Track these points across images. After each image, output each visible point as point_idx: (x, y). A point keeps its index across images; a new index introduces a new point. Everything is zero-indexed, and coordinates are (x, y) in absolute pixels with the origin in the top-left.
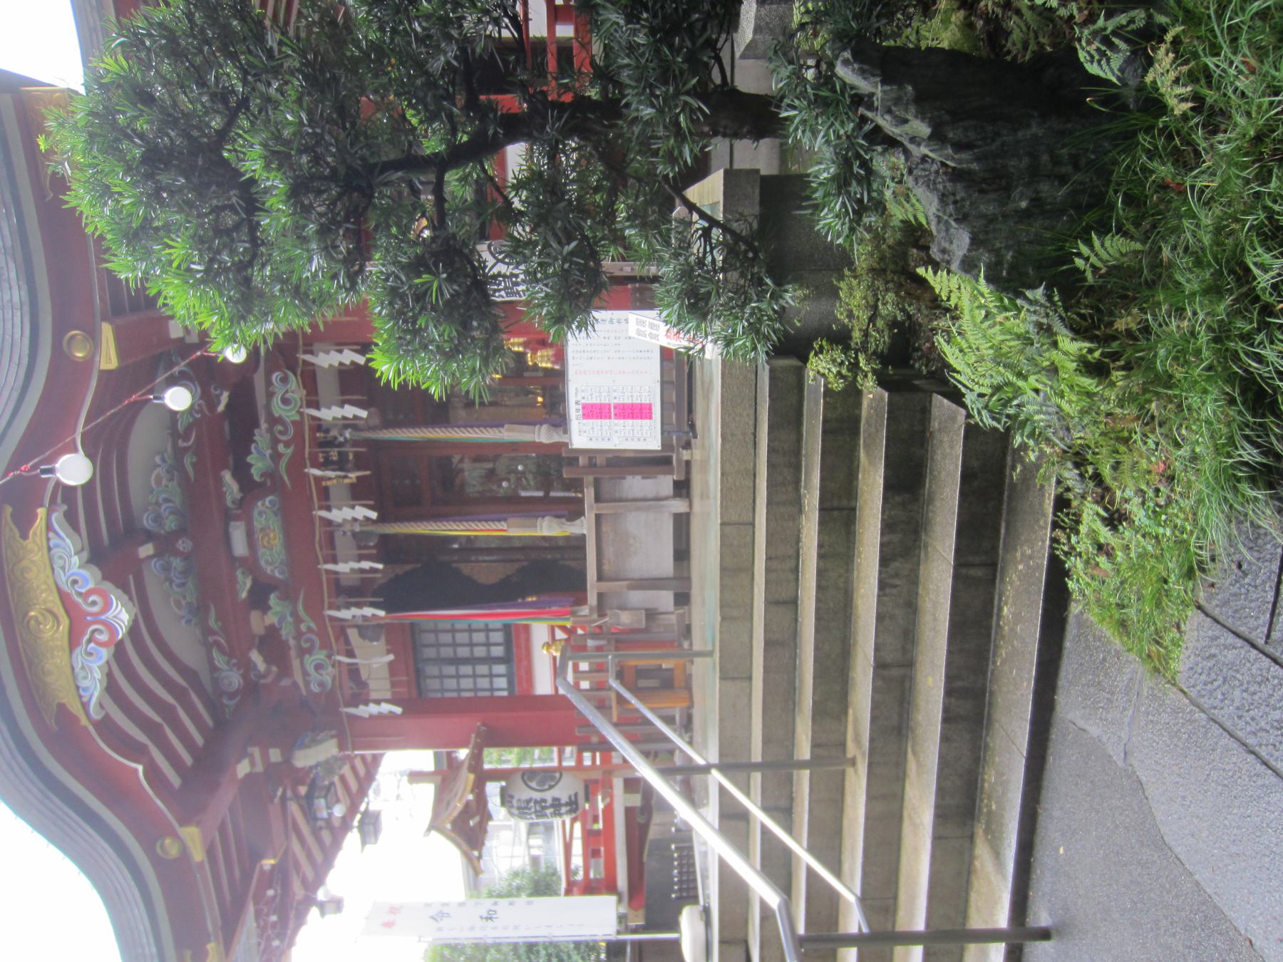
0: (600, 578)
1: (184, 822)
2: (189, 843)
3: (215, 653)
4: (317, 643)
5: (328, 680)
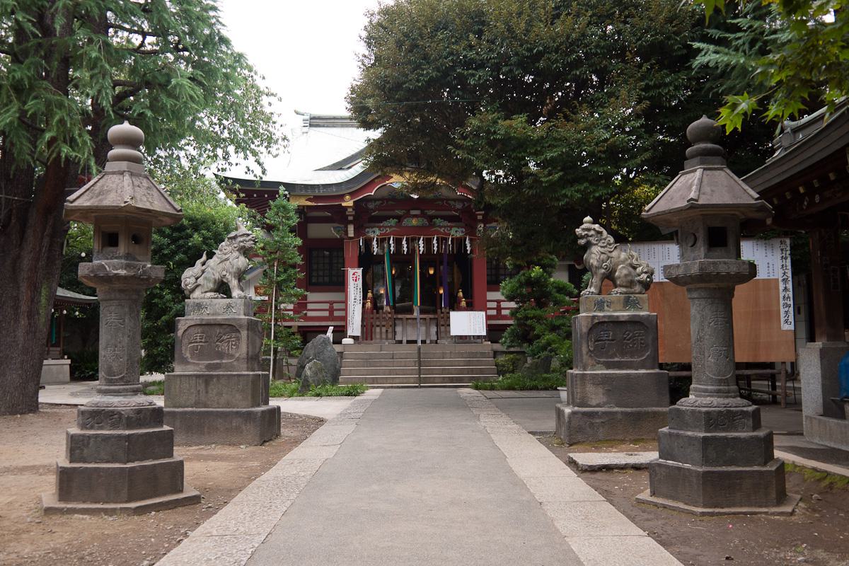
0: (407, 319)
3: (381, 202)
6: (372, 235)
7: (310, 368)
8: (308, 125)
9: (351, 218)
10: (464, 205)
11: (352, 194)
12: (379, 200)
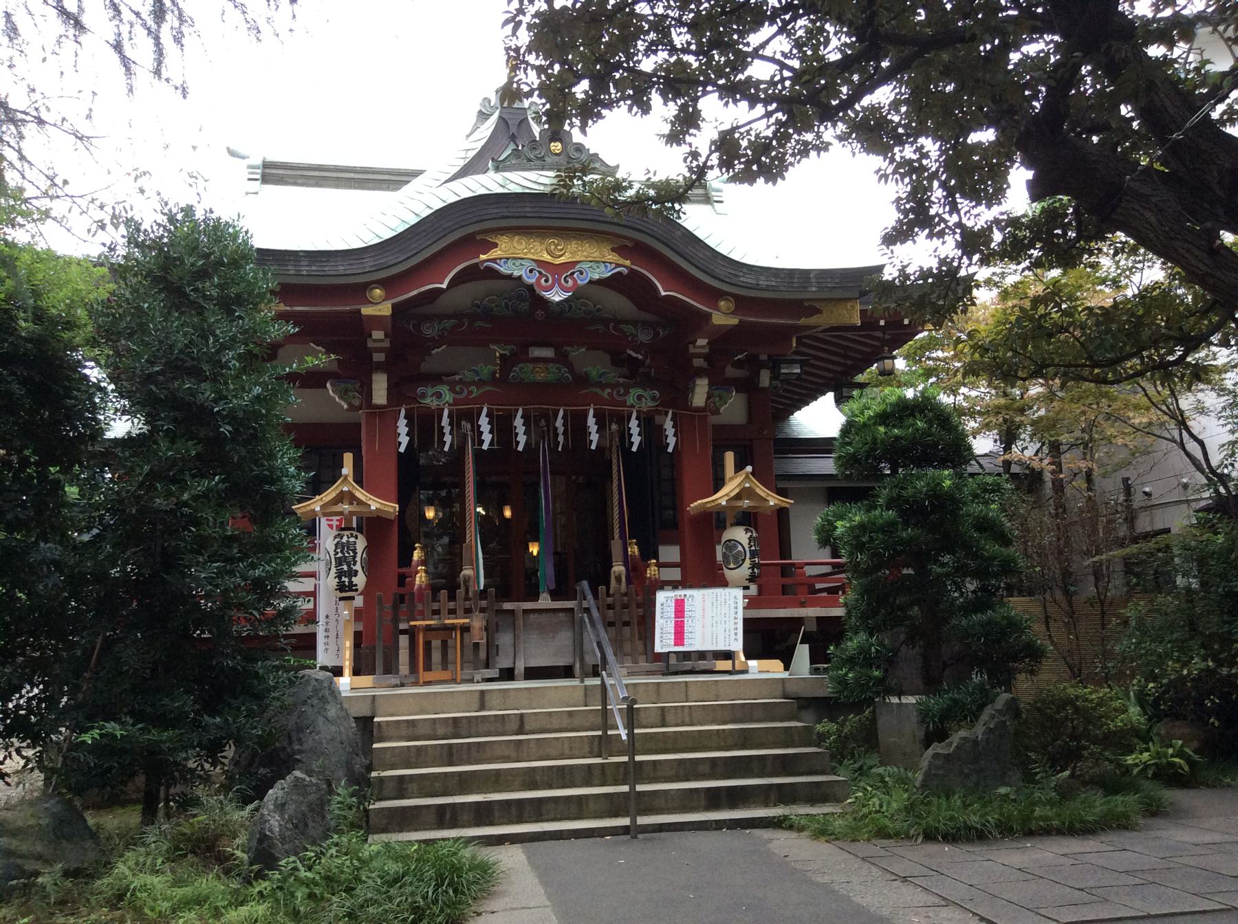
0: (526, 612)
1: (394, 306)
2: (379, 307)
4: (458, 396)
5: (428, 401)
6: (431, 402)
7: (281, 807)
8: (258, 177)
9: (379, 357)
10: (656, 334)
11: (390, 284)
12: (449, 317)
